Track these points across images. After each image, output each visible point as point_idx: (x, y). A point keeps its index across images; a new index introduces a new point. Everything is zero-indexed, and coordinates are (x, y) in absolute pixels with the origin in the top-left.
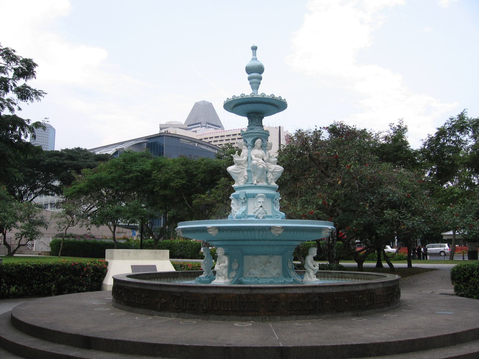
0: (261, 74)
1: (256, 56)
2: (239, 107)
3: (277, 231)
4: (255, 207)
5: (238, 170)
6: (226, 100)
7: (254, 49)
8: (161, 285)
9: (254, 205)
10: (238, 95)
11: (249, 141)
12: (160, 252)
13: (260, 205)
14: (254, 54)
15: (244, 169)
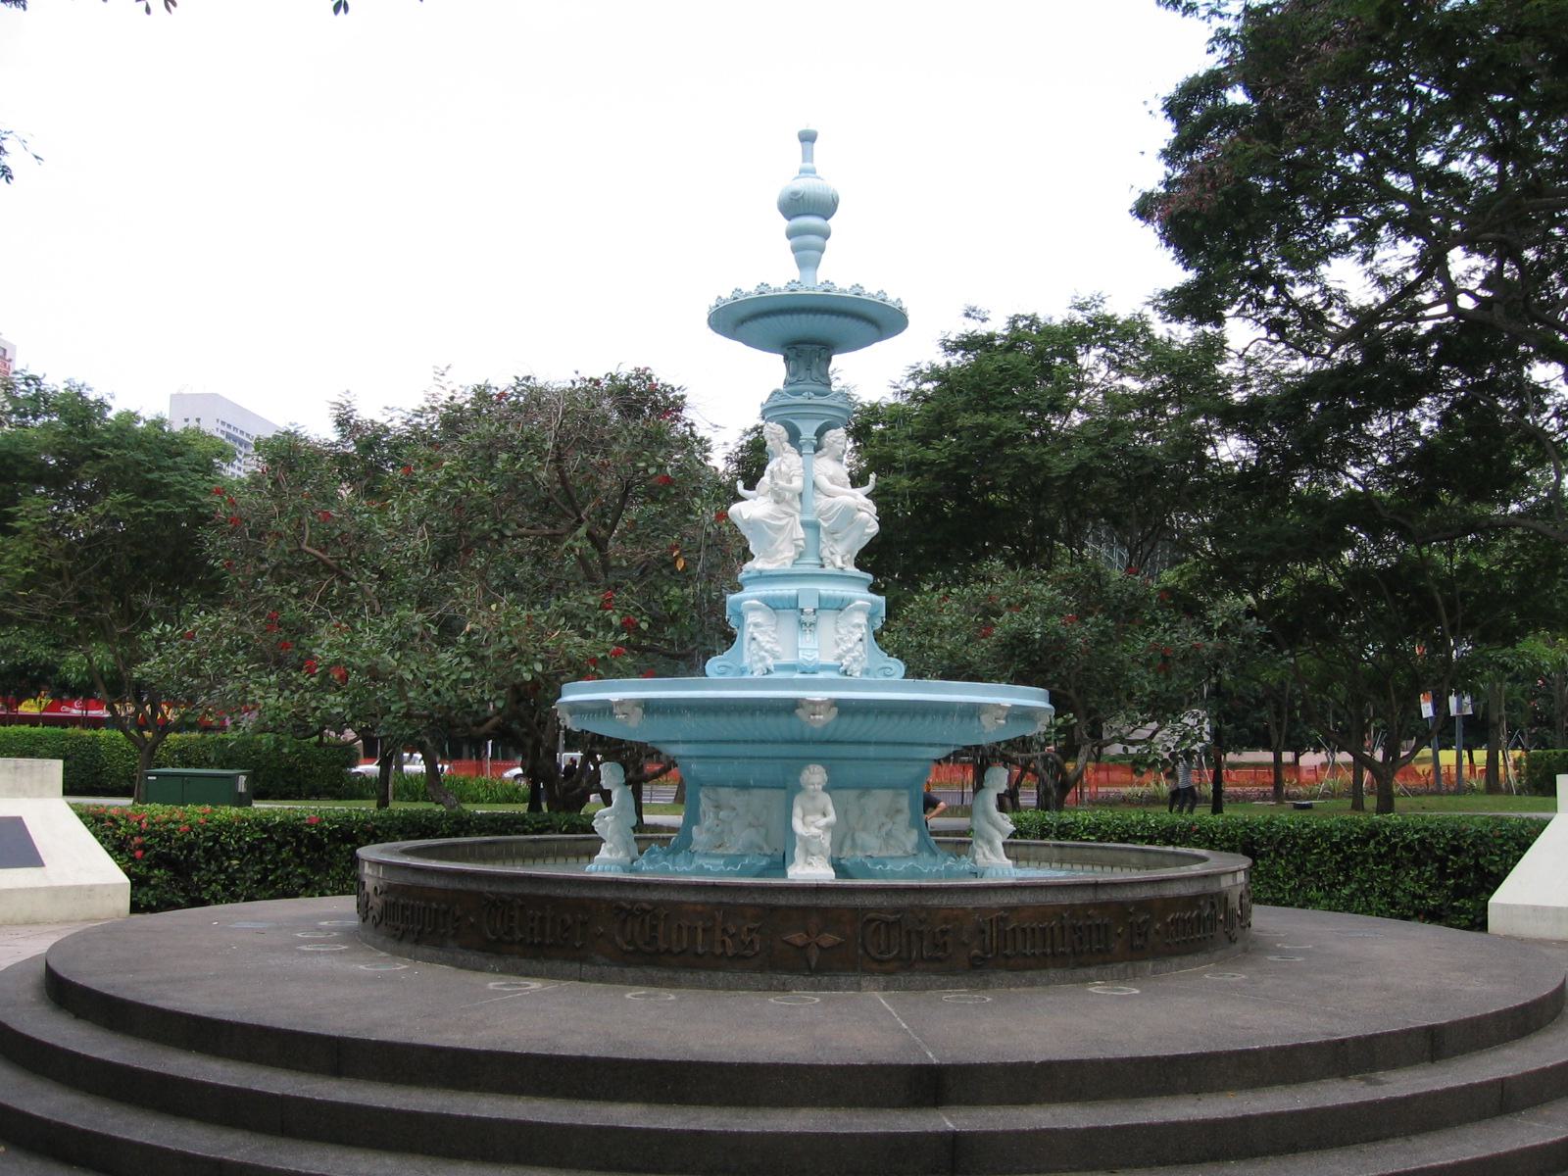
0: (826, 219)
1: (812, 161)
2: (754, 326)
3: (814, 715)
4: (841, 639)
5: (780, 519)
6: (714, 304)
7: (808, 138)
8: (531, 879)
9: (838, 632)
10: (750, 287)
11: (808, 431)
12: (32, 767)
13: (859, 635)
14: (807, 156)
15: (792, 515)
